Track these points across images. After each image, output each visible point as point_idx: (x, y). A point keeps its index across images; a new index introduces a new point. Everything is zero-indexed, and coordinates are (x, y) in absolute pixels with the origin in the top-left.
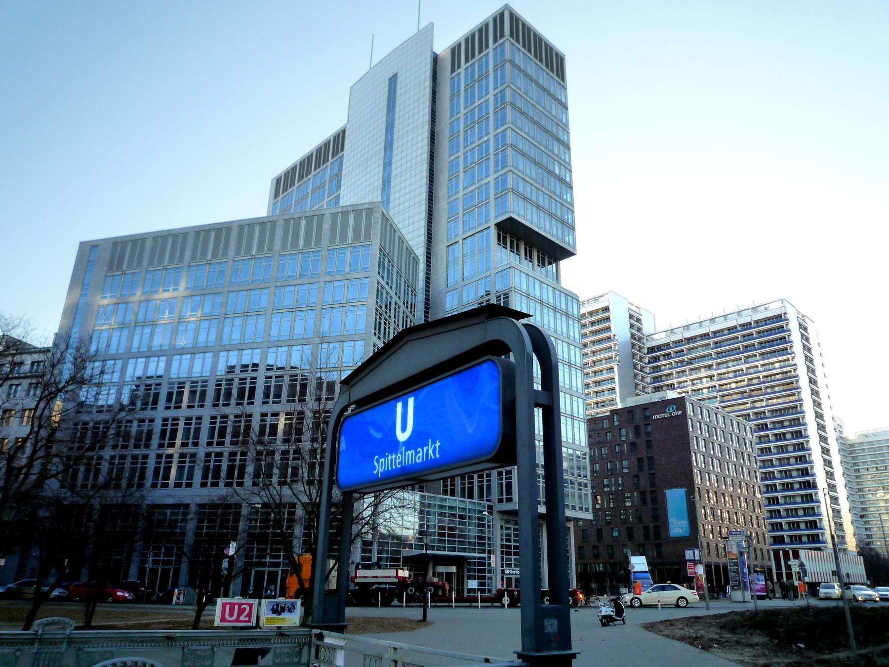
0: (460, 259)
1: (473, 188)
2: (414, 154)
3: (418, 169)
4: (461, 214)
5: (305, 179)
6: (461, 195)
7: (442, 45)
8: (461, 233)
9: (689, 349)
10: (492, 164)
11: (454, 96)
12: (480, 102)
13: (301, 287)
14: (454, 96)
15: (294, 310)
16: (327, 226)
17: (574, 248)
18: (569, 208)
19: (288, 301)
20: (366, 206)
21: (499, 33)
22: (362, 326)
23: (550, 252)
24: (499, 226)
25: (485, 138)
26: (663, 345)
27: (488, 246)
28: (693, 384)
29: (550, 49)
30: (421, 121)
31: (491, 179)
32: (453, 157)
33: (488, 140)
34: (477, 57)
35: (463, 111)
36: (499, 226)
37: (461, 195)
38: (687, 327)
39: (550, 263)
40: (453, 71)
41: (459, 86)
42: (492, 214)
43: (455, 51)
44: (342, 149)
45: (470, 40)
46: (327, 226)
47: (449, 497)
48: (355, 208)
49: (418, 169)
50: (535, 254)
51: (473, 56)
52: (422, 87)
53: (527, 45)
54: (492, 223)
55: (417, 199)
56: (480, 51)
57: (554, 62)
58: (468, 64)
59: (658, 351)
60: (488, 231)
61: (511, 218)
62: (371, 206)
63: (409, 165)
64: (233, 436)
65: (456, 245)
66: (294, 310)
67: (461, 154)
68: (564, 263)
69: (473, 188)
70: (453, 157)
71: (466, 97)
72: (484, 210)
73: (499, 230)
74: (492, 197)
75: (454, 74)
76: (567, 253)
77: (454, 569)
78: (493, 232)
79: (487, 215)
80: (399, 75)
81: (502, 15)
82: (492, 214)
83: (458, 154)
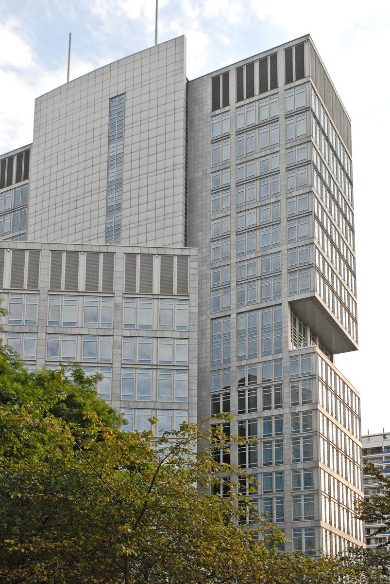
7: (198, 65)
8: (233, 306)
43: (219, 80)
44: (26, 177)
45: (245, 69)
54: (285, 301)
80: (128, 96)
82: (285, 290)
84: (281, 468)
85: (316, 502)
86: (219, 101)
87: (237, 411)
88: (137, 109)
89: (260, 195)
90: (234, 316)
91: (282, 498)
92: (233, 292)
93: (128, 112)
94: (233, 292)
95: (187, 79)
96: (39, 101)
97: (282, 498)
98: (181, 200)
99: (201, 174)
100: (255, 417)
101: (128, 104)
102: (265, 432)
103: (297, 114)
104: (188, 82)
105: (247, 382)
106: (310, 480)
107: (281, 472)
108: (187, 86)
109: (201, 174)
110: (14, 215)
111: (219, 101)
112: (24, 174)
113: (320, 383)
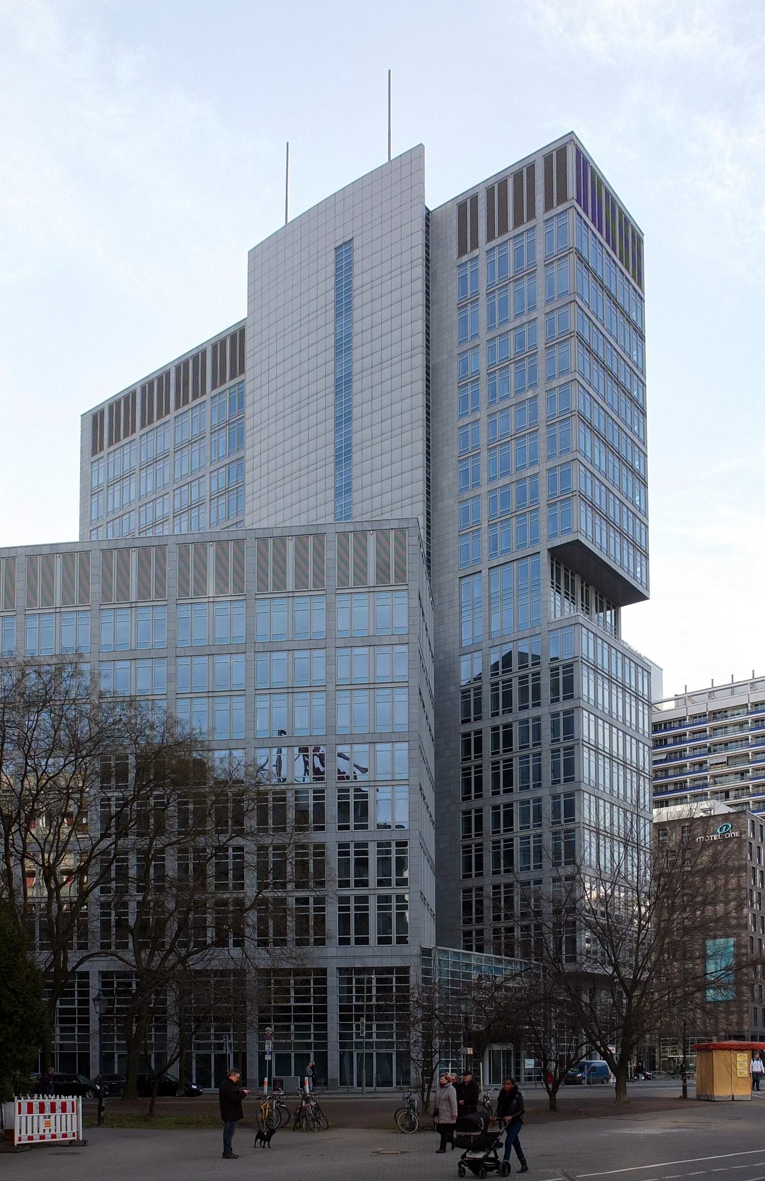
0: (486, 601)
1: (506, 480)
2: (397, 408)
3: (407, 436)
4: (485, 525)
5: (157, 423)
6: (484, 489)
7: (441, 190)
8: (485, 558)
9: (715, 729)
10: (542, 445)
11: (467, 302)
12: (517, 323)
13: (297, 654)
14: (467, 302)
15: (291, 690)
16: (331, 554)
17: (647, 588)
18: (641, 516)
19: (279, 676)
20: (395, 525)
21: (556, 194)
22: (402, 718)
23: (611, 589)
24: (554, 552)
25: (530, 394)
26: (675, 720)
27: (537, 585)
28: (715, 783)
29: (626, 221)
30: (407, 344)
31: (542, 468)
32: (467, 420)
33: (535, 397)
34: (512, 232)
35: (484, 336)
36: (554, 552)
37: (484, 489)
38: (711, 693)
39: (608, 609)
40: (462, 251)
41: (475, 285)
42: (544, 531)
43: (465, 207)
44: (242, 371)
45: (496, 189)
46: (331, 554)
47: (474, 953)
48: (376, 526)
49: (407, 436)
50: (592, 597)
51: (504, 229)
52: (407, 277)
53: (597, 219)
54: (543, 548)
55: (407, 490)
56: (518, 222)
57: (623, 240)
58: (493, 243)
59: (666, 729)
60: (535, 559)
61: (577, 542)
62: (404, 525)
63: (387, 425)
64: (217, 877)
65: (476, 577)
66: (291, 690)
67: (482, 415)
68: (626, 611)
69: (506, 480)
70: (467, 420)
71: (491, 308)
72: (528, 522)
73: (552, 559)
74: (543, 503)
75: (465, 258)
76: (636, 595)
77: (510, 1047)
78: (545, 560)
79: (535, 533)
80: (357, 243)
81: (562, 152)
82: (544, 531)
83: (478, 415)
84: (539, 793)
85: (576, 756)
86: (466, 242)
87: (491, 831)
88: (367, 349)
89: (517, 582)
90: (485, 572)
91: (540, 754)
92: (485, 536)
93: (357, 269)
94: (485, 536)
95: (426, 208)
96: (255, 255)
97: (540, 836)
98: (420, 450)
99: (446, 356)
100: (510, 720)
101: (357, 256)
102: (521, 742)
103: (559, 259)
104: (428, 212)
105: (501, 670)
106: (570, 810)
107: (539, 800)
108: (427, 219)
109: (446, 356)
110: (230, 429)
111: (466, 242)
112: (238, 367)
113: (587, 832)
